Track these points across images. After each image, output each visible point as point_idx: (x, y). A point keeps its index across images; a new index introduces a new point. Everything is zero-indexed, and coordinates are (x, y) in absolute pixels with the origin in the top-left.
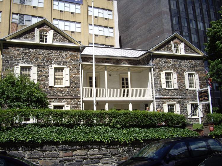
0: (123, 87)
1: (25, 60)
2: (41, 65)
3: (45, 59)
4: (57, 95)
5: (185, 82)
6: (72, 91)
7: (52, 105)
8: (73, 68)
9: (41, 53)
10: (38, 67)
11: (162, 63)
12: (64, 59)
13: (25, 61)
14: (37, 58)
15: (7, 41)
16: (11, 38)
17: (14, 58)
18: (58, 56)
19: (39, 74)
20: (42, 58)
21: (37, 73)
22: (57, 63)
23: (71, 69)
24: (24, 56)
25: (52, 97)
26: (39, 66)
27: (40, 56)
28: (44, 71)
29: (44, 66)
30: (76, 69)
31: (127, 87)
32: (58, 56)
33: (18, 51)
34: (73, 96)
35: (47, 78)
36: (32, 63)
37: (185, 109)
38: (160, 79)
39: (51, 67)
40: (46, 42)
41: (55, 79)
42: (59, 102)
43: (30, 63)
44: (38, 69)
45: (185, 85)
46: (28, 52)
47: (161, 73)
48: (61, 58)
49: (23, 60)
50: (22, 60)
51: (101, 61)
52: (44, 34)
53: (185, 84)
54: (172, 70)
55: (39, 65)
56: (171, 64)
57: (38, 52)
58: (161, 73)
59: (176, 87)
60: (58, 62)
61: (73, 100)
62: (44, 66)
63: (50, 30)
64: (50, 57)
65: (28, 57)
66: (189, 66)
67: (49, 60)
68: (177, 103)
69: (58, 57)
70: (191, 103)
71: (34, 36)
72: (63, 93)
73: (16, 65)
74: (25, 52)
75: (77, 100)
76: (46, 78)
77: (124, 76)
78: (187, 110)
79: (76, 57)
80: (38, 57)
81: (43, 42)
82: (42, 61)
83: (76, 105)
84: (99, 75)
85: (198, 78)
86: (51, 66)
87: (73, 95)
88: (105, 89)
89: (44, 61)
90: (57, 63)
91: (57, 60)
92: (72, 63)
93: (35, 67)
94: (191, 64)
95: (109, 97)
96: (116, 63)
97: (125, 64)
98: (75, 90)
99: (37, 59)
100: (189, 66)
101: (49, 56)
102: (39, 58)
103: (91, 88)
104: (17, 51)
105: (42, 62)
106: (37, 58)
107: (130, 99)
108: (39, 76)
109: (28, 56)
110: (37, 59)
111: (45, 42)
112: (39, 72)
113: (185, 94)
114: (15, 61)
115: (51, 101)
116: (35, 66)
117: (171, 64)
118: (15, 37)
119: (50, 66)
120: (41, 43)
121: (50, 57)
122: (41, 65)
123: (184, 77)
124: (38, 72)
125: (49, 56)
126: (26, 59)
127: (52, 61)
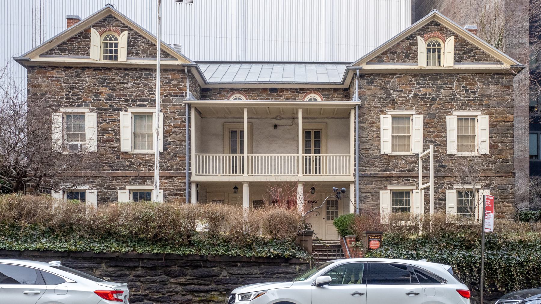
0: (233, 150)
1: (72, 99)
2: (105, 110)
3: (113, 96)
4: (138, 171)
5: (445, 137)
6: (168, 160)
7: (454, 189)
8: (171, 113)
9: (104, 83)
10: (99, 114)
11: (387, 92)
12: (152, 94)
13: (73, 102)
14: (97, 94)
15: (32, 60)
16: (43, 54)
17: (50, 96)
18: (141, 87)
19: (100, 127)
20: (107, 95)
21: (98, 126)
22: (138, 103)
23: (168, 115)
24: (70, 92)
25: (128, 173)
26: (101, 111)
27: (102, 89)
28: (112, 121)
29: (111, 110)
30: (178, 115)
31: (242, 151)
32: (141, 87)
33: (58, 81)
34: (172, 171)
35: (118, 134)
36: (86, 105)
37: (441, 204)
38: (379, 131)
39: (126, 113)
40: (116, 58)
41: (136, 136)
42: (142, 183)
43: (82, 105)
44: (98, 118)
45: (446, 145)
46: (77, 82)
47: (382, 116)
48: (146, 92)
49: (69, 99)
50: (67, 99)
51: (258, 96)
52: (107, 40)
53: (446, 141)
54: (414, 108)
55: (102, 109)
56: (411, 96)
57: (99, 81)
58: (382, 116)
59: (485, 149)
60: (140, 100)
61: (170, 180)
62: (111, 110)
63: (122, 32)
64: (123, 90)
65: (78, 92)
66: (466, 97)
67: (121, 98)
68: (482, 188)
69: (140, 91)
70: (391, 190)
71: (90, 48)
72: (149, 166)
73: (56, 111)
74: (73, 83)
75: (178, 179)
76: (116, 135)
77: (234, 126)
78: (445, 204)
79: (179, 88)
80: (98, 93)
81: (111, 58)
82: (106, 100)
83: (176, 190)
84: (327, 127)
85: (86, 119)
86: (126, 111)
87: (171, 170)
88: (350, 157)
89: (110, 100)
90: (138, 103)
91: (139, 96)
92: (170, 102)
93: (92, 113)
94: (472, 92)
95: (250, 174)
96: (292, 99)
97: (239, 99)
98: (175, 158)
99: (97, 96)
100: (466, 97)
101: (120, 90)
102: (100, 93)
103: (318, 155)
104: (55, 81)
105: (107, 103)
106: (97, 94)
107: (245, 177)
108: (101, 132)
109: (78, 91)
110: (97, 96)
111: (109, 60)
112: (101, 123)
113: (445, 166)
114: (53, 101)
115: (126, 182)
116: (92, 111)
117: (411, 96)
118: (50, 53)
119: (123, 111)
120: (108, 62)
121: (123, 90)
122: (105, 110)
123: (444, 125)
124: (98, 122)
125: (120, 90)
126: (74, 98)
127: (127, 100)
